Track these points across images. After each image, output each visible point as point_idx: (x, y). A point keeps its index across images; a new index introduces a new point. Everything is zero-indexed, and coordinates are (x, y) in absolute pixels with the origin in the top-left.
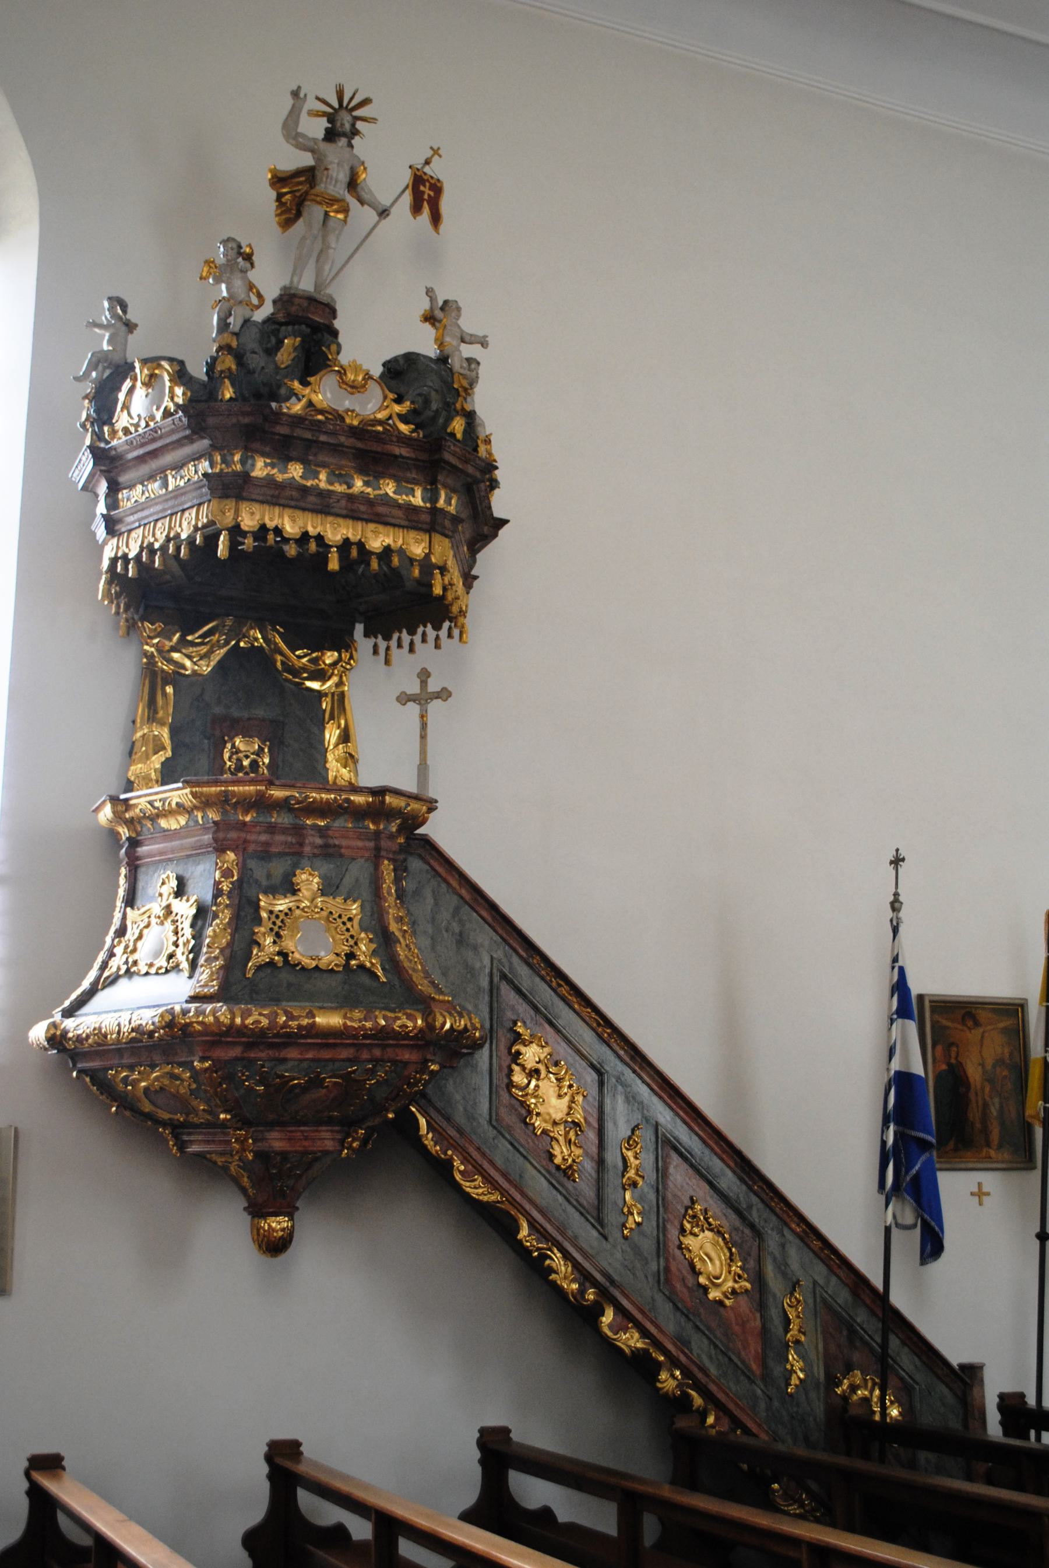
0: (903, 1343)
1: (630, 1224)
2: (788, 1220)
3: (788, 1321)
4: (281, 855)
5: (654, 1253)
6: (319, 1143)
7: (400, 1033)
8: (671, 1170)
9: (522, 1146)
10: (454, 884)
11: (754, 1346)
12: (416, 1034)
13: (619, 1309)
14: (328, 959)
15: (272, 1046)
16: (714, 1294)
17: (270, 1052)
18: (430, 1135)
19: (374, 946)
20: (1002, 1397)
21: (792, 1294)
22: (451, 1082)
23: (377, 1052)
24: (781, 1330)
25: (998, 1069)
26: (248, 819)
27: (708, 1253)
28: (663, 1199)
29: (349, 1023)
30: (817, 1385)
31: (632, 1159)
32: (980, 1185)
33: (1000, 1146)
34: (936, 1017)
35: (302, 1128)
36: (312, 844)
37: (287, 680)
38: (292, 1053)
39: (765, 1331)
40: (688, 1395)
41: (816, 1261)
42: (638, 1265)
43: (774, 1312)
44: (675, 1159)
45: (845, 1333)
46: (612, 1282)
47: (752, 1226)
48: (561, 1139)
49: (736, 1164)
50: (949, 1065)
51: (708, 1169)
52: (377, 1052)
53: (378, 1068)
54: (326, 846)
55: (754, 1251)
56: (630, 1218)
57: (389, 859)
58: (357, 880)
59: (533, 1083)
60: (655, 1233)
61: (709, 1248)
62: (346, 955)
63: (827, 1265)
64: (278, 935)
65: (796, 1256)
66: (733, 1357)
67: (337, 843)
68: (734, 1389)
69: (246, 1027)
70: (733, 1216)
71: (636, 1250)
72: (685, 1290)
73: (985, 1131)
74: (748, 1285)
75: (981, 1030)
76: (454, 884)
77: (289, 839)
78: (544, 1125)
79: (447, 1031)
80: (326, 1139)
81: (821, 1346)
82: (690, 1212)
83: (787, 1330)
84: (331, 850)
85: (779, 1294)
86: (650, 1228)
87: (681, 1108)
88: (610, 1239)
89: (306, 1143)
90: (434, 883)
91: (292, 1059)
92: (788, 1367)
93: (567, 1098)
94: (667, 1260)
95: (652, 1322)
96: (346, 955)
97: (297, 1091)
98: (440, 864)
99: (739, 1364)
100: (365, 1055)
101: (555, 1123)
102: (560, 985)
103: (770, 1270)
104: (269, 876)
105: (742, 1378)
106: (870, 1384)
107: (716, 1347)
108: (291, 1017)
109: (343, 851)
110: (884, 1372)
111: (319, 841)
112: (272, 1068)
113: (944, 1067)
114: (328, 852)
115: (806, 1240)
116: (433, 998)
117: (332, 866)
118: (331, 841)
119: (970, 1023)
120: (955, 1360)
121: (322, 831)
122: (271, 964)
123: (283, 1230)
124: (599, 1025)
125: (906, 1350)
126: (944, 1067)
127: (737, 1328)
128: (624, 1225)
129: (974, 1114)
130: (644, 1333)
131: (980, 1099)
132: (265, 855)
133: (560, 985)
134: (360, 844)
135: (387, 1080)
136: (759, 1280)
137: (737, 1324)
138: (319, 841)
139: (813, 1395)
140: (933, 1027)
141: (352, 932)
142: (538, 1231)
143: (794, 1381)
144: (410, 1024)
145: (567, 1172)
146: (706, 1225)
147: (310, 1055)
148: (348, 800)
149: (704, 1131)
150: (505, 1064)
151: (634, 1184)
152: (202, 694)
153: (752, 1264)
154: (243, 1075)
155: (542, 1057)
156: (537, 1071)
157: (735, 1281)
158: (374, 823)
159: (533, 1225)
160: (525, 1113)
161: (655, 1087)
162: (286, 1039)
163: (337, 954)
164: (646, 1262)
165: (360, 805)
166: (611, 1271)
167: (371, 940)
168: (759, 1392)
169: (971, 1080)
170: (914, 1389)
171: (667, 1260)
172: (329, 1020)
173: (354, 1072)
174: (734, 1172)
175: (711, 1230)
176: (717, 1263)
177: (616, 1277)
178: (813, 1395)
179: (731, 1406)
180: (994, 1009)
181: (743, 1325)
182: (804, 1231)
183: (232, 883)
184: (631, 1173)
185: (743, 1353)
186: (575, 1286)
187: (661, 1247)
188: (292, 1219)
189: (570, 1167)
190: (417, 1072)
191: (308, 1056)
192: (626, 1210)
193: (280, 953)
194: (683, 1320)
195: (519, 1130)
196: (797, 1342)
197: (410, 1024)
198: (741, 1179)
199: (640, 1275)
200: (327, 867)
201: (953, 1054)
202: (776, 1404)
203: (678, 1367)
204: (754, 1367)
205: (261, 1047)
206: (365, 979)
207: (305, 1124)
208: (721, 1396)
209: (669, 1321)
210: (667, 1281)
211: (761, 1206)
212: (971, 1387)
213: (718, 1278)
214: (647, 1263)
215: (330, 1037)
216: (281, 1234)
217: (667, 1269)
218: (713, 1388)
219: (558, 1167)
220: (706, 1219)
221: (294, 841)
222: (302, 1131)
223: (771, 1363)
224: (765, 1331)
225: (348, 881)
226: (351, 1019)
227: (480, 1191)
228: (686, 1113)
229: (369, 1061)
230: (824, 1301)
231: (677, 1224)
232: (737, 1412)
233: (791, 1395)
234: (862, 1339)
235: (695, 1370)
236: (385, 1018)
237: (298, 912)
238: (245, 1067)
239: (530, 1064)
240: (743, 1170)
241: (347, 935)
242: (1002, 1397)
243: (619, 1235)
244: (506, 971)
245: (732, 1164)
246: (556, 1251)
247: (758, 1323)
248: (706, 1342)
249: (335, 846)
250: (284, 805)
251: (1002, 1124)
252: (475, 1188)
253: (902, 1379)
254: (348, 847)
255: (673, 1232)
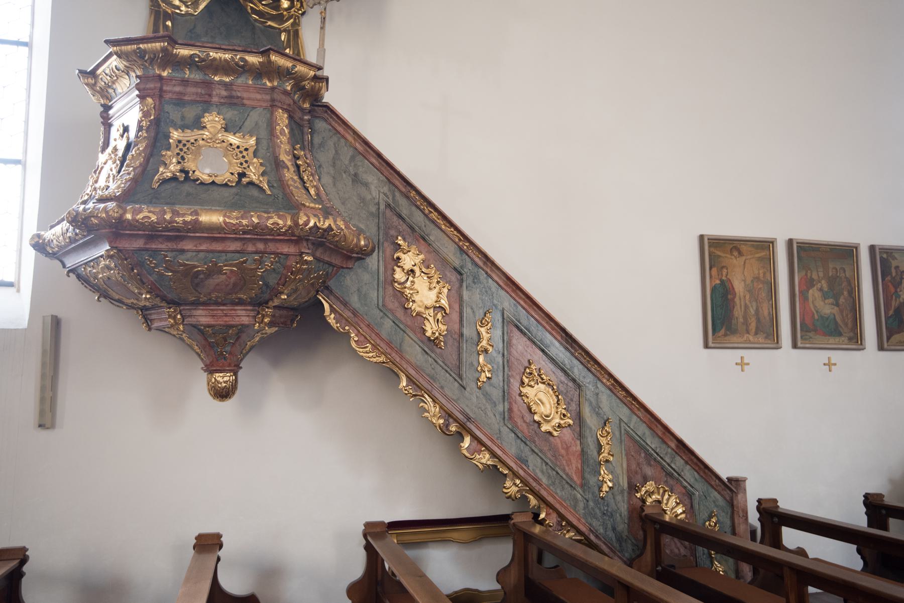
0: (687, 463)
1: (483, 378)
2: (601, 377)
3: (600, 447)
4: (194, 102)
5: (501, 398)
6: (237, 319)
7: (272, 229)
8: (514, 341)
9: (403, 323)
10: (350, 138)
11: (576, 464)
12: (287, 231)
13: (474, 437)
14: (224, 176)
15: (169, 239)
16: (545, 427)
17: (169, 244)
18: (333, 316)
19: (262, 169)
20: (760, 501)
21: (603, 428)
22: (348, 278)
23: (261, 246)
24: (595, 453)
25: (755, 284)
26: (165, 74)
27: (543, 400)
28: (508, 361)
29: (227, 220)
30: (622, 492)
31: (484, 334)
32: (742, 358)
33: (756, 334)
34: (712, 249)
35: (222, 308)
36: (219, 96)
37: (256, 20)
38: (188, 245)
39: (583, 453)
40: (527, 498)
41: (621, 405)
42: (489, 407)
43: (590, 441)
44: (516, 334)
45: (643, 455)
46: (469, 419)
47: (574, 381)
48: (431, 319)
49: (562, 337)
50: (721, 280)
51: (541, 341)
52: (261, 246)
53: (264, 259)
54: (230, 97)
55: (576, 398)
56: (483, 374)
57: (283, 109)
58: (257, 124)
59: (411, 278)
60: (501, 384)
61: (542, 396)
62: (239, 174)
63: (630, 409)
64: (183, 158)
65: (607, 401)
66: (559, 471)
67: (239, 94)
68: (560, 494)
69: (137, 221)
70: (560, 374)
71: (486, 395)
72: (524, 425)
73: (746, 323)
74: (571, 422)
75: (744, 258)
76: (350, 138)
77: (199, 90)
78: (418, 309)
79: (311, 228)
80: (243, 316)
81: (625, 465)
82: (528, 370)
83: (599, 453)
84: (235, 101)
85: (593, 428)
86: (498, 380)
87: (521, 298)
88: (468, 389)
89: (227, 319)
90: (335, 139)
91: (188, 251)
92: (601, 478)
93: (435, 291)
94: (510, 403)
95: (499, 447)
96: (239, 174)
97: (202, 276)
98: (339, 125)
99: (564, 476)
100: (251, 248)
101: (427, 308)
102: (431, 212)
103: (587, 412)
104: (183, 118)
105: (566, 486)
106: (661, 491)
107: (547, 464)
108: (175, 213)
109: (245, 102)
110: (670, 479)
111: (224, 93)
112: (175, 258)
113: (718, 282)
114: (232, 101)
115: (615, 391)
116: (304, 205)
117: (236, 112)
118: (234, 93)
119: (736, 253)
120: (724, 476)
121: (226, 85)
122: (174, 179)
123: (225, 382)
124: (460, 240)
125: (688, 467)
126: (718, 282)
127: (563, 452)
128: (478, 379)
129: (738, 312)
130: (494, 455)
131: (743, 303)
132: (180, 102)
133: (431, 212)
134: (259, 96)
135: (274, 269)
136: (579, 418)
137: (563, 448)
138: (224, 93)
139: (619, 498)
140: (710, 255)
141: (247, 158)
142: (415, 383)
143: (605, 488)
144: (281, 222)
145: (433, 342)
146: (540, 380)
147: (203, 247)
148: (242, 59)
149: (538, 314)
150: (390, 267)
151: (486, 351)
152: (195, 27)
153: (574, 406)
154: (151, 262)
155: (417, 262)
156: (412, 271)
157: (561, 419)
158: (270, 81)
159: (410, 379)
160: (403, 299)
161: (501, 284)
162: (178, 234)
163: (232, 174)
164: (495, 405)
165: (253, 64)
166: (468, 410)
167: (261, 164)
168: (579, 496)
169: (736, 290)
170: (694, 494)
171: (510, 403)
172: (212, 218)
173: (245, 262)
174: (561, 344)
175: (544, 383)
176: (548, 406)
177: (471, 415)
178: (619, 498)
179: (558, 506)
180: (753, 246)
181: (567, 449)
182: (612, 385)
183: (150, 121)
184: (484, 343)
185: (567, 468)
186: (441, 421)
187: (506, 395)
188: (235, 374)
189: (437, 338)
190: (297, 263)
191: (202, 248)
192: (479, 368)
193: (182, 171)
194: (523, 445)
195: (400, 313)
196: (607, 461)
197: (281, 222)
198: (566, 349)
199: (490, 414)
200: (231, 113)
201: (724, 274)
202: (591, 504)
203: (518, 478)
204: (575, 478)
205: (160, 240)
206: (255, 192)
207: (224, 305)
208: (550, 499)
209: (510, 447)
210: (511, 418)
211: (581, 367)
212: (737, 494)
213: (548, 416)
214: (495, 406)
215: (215, 234)
216: (224, 385)
217: (510, 410)
218: (544, 493)
219: (429, 338)
220: (539, 375)
221: (203, 92)
222: (222, 310)
223: (587, 476)
224: (583, 453)
225: (249, 124)
226: (229, 217)
227: (371, 355)
228: (525, 302)
229: (256, 253)
230: (627, 433)
231: (518, 378)
232: (562, 511)
233: (602, 498)
234: (655, 459)
235: (531, 481)
236: (259, 217)
237: (201, 142)
238: (150, 256)
239: (407, 267)
240: (567, 342)
241: (242, 160)
242: (760, 501)
243: (474, 386)
244: (390, 202)
245: (559, 338)
246: (427, 396)
247: (579, 448)
248: (539, 461)
249: (238, 97)
250: (189, 62)
251: (758, 320)
252: (367, 352)
253: (685, 487)
254: (249, 99)
255: (515, 384)
